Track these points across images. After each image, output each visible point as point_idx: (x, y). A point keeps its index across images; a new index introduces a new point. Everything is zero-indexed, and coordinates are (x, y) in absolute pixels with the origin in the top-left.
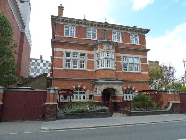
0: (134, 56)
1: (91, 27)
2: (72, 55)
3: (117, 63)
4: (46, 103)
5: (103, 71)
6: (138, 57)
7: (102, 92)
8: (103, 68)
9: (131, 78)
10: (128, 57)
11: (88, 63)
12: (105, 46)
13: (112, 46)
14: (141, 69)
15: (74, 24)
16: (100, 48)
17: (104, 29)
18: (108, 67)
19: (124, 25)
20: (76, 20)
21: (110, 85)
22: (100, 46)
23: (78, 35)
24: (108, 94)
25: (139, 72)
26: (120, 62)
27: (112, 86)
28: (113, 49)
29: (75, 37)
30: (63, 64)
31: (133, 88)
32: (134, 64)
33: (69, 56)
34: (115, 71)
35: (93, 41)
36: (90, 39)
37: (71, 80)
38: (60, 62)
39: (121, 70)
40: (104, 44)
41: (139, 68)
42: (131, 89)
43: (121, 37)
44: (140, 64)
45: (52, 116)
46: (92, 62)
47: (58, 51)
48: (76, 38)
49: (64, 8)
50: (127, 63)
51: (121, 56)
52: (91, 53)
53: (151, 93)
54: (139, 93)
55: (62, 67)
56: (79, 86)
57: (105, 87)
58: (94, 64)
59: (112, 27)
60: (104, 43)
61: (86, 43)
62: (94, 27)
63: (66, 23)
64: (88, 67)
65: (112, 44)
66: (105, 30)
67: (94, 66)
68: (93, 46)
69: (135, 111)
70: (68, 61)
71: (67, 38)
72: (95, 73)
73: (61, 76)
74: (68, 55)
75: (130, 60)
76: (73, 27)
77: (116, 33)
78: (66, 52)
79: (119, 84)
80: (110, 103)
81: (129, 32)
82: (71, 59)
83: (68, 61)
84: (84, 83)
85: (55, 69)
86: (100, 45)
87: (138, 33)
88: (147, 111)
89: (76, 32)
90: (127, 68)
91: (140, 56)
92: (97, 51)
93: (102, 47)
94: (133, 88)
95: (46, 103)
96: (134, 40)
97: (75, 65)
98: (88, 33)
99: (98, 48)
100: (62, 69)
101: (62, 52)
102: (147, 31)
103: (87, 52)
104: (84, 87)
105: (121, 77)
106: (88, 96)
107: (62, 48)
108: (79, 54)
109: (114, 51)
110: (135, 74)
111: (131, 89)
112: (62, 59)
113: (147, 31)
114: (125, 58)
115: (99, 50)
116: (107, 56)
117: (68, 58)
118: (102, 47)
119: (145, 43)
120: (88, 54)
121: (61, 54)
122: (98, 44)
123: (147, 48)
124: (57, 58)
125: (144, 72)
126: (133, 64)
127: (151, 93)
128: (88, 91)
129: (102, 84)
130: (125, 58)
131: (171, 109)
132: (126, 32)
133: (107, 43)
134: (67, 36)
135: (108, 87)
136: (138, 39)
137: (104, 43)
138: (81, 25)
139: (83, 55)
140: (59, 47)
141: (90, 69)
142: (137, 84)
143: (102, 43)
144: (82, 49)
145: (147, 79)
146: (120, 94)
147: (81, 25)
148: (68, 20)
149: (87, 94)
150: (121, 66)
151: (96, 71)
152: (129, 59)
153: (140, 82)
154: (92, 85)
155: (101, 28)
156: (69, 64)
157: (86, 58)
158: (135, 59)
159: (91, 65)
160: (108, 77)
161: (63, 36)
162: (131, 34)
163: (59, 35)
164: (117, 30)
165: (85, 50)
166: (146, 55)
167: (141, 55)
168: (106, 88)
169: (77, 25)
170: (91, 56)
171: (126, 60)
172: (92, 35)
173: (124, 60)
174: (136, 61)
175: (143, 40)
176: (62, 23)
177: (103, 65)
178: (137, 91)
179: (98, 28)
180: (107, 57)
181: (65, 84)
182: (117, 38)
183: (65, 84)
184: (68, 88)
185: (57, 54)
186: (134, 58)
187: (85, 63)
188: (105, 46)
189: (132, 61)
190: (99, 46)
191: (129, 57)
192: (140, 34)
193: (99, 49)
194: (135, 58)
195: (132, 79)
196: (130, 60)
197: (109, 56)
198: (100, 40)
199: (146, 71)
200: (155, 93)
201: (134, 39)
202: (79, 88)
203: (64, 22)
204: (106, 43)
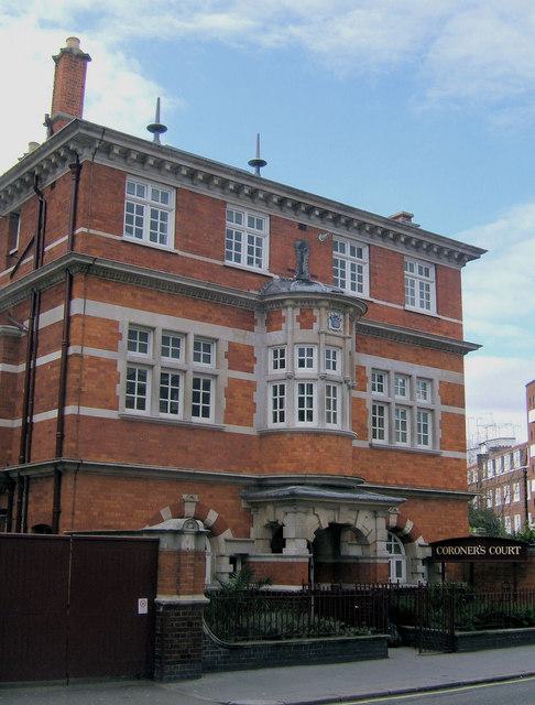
0: (417, 370)
5: (308, 439)
8: (306, 424)
9: (403, 477)
11: (229, 394)
12: (323, 319)
17: (303, 219)
19: (329, 198)
20: (280, 190)
22: (297, 312)
23: (187, 236)
25: (428, 448)
29: (170, 246)
33: (176, 354)
34: (351, 438)
35: (255, 278)
36: (237, 265)
38: (102, 375)
40: (286, 307)
41: (434, 428)
45: (189, 656)
48: (180, 253)
49: (58, 53)
53: (440, 550)
54: (434, 552)
56: (409, 527)
57: (325, 518)
58: (257, 397)
59: (336, 219)
60: (317, 301)
61: (227, 289)
62: (261, 207)
64: (231, 415)
66: (302, 227)
67: (252, 408)
68: (257, 309)
73: (110, 454)
76: (161, 189)
77: (416, 269)
78: (130, 324)
79: (376, 509)
81: (400, 249)
84: (211, 496)
88: (249, 643)
89: (178, 225)
90: (212, 406)
92: (276, 337)
93: (306, 323)
96: (348, 272)
99: (283, 320)
101: (115, 324)
102: (476, 253)
103: (226, 334)
105: (362, 469)
107: (114, 300)
108: (159, 334)
112: (113, 364)
115: (290, 331)
116: (302, 364)
117: (201, 366)
118: (306, 323)
119: (458, 314)
120: (231, 345)
123: (466, 338)
124: (91, 357)
127: (440, 550)
128: (228, 534)
129: (310, 503)
132: (389, 246)
135: (332, 520)
138: (202, 190)
140: (99, 297)
141: (240, 422)
142: (422, 506)
143: (308, 300)
144: (204, 319)
146: (379, 555)
147: (202, 190)
148: (248, 183)
149: (223, 551)
153: (437, 499)
154: (244, 505)
155: (289, 216)
159: (241, 401)
160: (333, 470)
162: (129, 179)
164: (354, 235)
165: (218, 322)
166: (460, 368)
170: (241, 358)
172: (251, 243)
173: (132, 347)
178: (420, 540)
179: (186, 185)
180: (328, 371)
187: (212, 392)
188: (323, 319)
190: (290, 314)
192: (444, 262)
195: (402, 479)
197: (310, 365)
200: (510, 550)
204: (327, 304)
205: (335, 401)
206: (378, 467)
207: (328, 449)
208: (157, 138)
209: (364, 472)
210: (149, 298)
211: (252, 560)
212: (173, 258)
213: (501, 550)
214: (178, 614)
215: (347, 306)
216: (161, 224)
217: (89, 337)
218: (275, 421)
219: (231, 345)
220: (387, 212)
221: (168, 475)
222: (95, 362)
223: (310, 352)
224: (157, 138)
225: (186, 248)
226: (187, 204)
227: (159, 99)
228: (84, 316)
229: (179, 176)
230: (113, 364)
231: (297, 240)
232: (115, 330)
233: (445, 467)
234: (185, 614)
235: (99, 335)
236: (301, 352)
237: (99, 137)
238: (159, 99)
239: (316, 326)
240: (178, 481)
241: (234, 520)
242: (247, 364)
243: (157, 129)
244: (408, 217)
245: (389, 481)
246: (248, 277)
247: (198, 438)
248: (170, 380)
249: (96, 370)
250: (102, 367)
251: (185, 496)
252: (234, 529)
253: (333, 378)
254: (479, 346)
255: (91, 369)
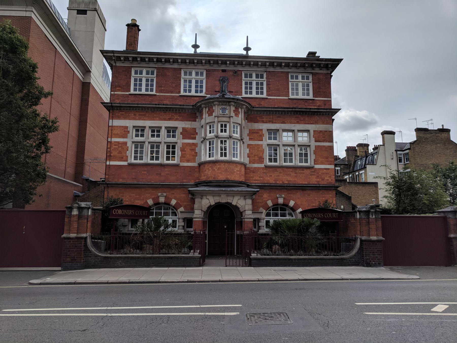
0: (297, 127)
1: (191, 66)
2: (148, 132)
3: (252, 145)
4: (64, 235)
6: (293, 128)
7: (205, 213)
9: (285, 179)
10: (281, 131)
11: (182, 150)
12: (217, 110)
13: (233, 108)
14: (313, 157)
15: (152, 65)
16: (207, 115)
17: (223, 67)
18: (234, 157)
19: (329, 58)
21: (222, 196)
22: (207, 109)
23: (161, 87)
24: (222, 216)
26: (260, 143)
27: (229, 198)
28: (237, 115)
30: (128, 153)
31: (292, 203)
32: (296, 146)
33: (158, 136)
36: (190, 94)
37: (143, 188)
38: (120, 148)
39: (261, 160)
40: (215, 105)
42: (167, 204)
43: (265, 83)
44: (311, 146)
45: (76, 260)
46: (193, 147)
47: (117, 126)
48: (158, 94)
50: (279, 145)
51: (262, 130)
52: (189, 126)
55: (127, 161)
56: (162, 200)
60: (213, 102)
62: (200, 67)
63: (135, 64)
64: (182, 158)
65: (233, 103)
66: (224, 71)
68: (194, 110)
69: (265, 255)
70: (139, 145)
71: (138, 96)
72: (199, 171)
74: (156, 133)
75: (287, 138)
76: (150, 70)
79: (245, 195)
80: (222, 237)
81: (176, 66)
82: (144, 142)
83: (139, 145)
84: (173, 194)
85: (111, 164)
86: (206, 108)
87: (310, 70)
91: (312, 127)
92: (203, 122)
94: (292, 203)
95: (64, 235)
97: (155, 154)
98: (185, 81)
100: (125, 163)
103: (180, 125)
104: (173, 202)
105: (260, 177)
106: (181, 220)
107: (125, 118)
109: (240, 118)
110: (298, 171)
111: (167, 204)
112: (125, 143)
113: (333, 64)
114: (274, 133)
115: (206, 118)
117: (155, 139)
118: (210, 114)
120: (183, 128)
121: (125, 132)
122: (203, 106)
123: (333, 107)
124: (115, 142)
125: (322, 163)
126: (294, 146)
127: (115, 212)
128: (182, 209)
129: (202, 195)
130: (275, 134)
131: (355, 254)
133: (219, 102)
134: (138, 92)
135: (217, 201)
136: (311, 85)
137: (213, 102)
138: (167, 66)
139: (140, 130)
140: (119, 118)
141: (188, 161)
144: (169, 119)
145: (330, 179)
150: (263, 151)
151: (200, 164)
152: (285, 134)
153: (310, 190)
155: (216, 67)
156: (158, 152)
157: (179, 140)
158: (300, 134)
159: (191, 151)
160: (222, 177)
161: (127, 93)
163: (119, 90)
164: (255, 68)
165: (177, 120)
167: (316, 123)
168: (213, 203)
169: (160, 65)
171: (275, 138)
172: (193, 85)
174: (303, 138)
175: (323, 87)
176: (127, 64)
177: (223, 151)
179: (207, 67)
181: (131, 195)
182: (253, 89)
183: (131, 195)
184: (139, 203)
185: (114, 132)
186: (296, 131)
188: (217, 110)
189: (294, 137)
190: (205, 111)
191: (284, 130)
193: (240, 116)
194: (299, 131)
195: (288, 181)
196: (287, 138)
197: (225, 132)
198: (211, 94)
199: (328, 161)
201: (300, 85)
202: (280, 204)
203: (219, 65)
204: (216, 103)
205: (237, 148)
206: (271, 176)
207: (219, 169)
208: (247, 53)
209: (262, 179)
210: (142, 115)
211: (245, 220)
212: (154, 97)
213: (330, 215)
214: (70, 242)
215: (229, 102)
216: (189, 85)
217: (114, 134)
218: (210, 157)
219: (183, 128)
220: (304, 55)
221: (153, 186)
222: (117, 144)
223: (226, 126)
224: (247, 53)
225: (160, 91)
226: (161, 74)
227: (247, 37)
228: (112, 126)
229: (282, 67)
230: (125, 143)
231: (221, 77)
232: (126, 130)
233: (318, 173)
234: (73, 242)
235: (119, 133)
236: (222, 126)
237: (112, 55)
238: (247, 37)
239: (214, 114)
240: (156, 188)
241: (185, 203)
242: (192, 136)
243: (196, 46)
244: (315, 53)
245: (278, 182)
246: (193, 98)
247: (166, 169)
248: (155, 146)
249: (117, 147)
250: (120, 145)
251: (159, 194)
252: (185, 207)
253: (222, 136)
254: (340, 109)
255: (115, 147)
